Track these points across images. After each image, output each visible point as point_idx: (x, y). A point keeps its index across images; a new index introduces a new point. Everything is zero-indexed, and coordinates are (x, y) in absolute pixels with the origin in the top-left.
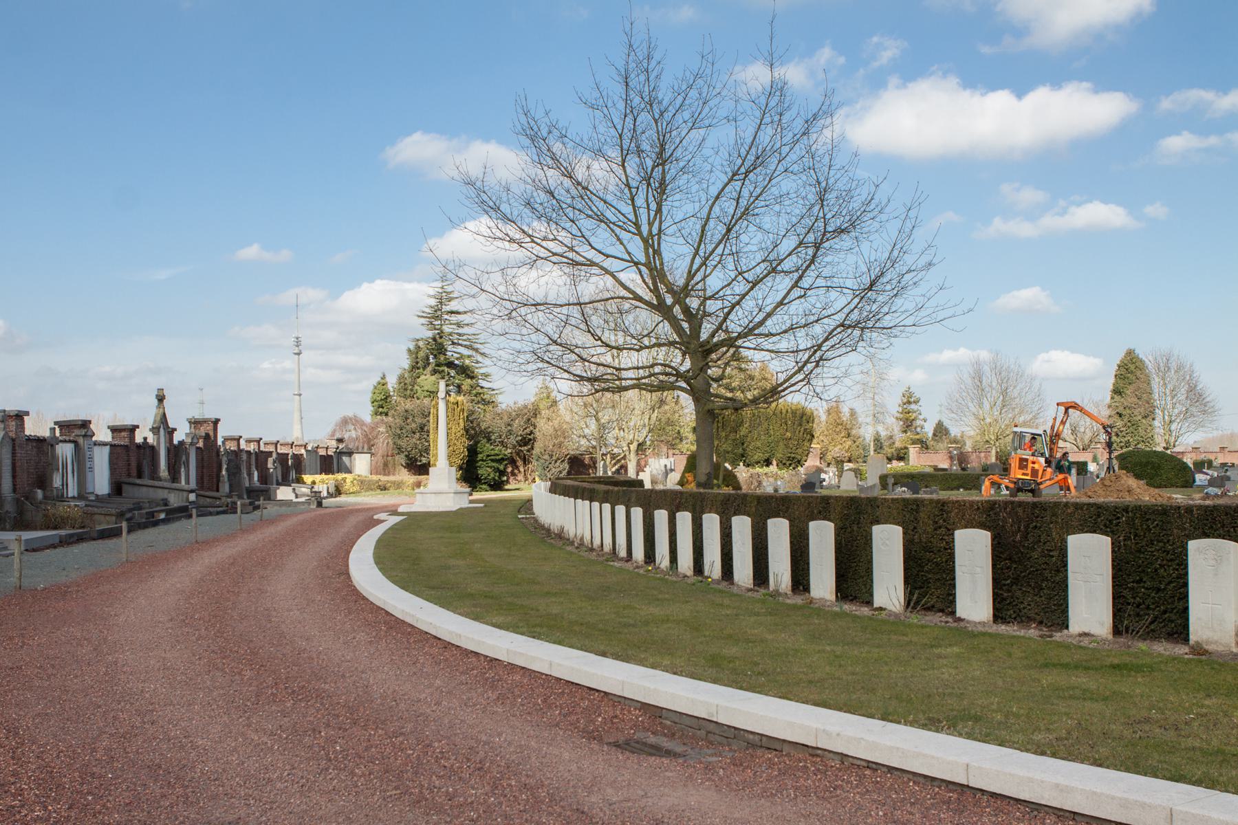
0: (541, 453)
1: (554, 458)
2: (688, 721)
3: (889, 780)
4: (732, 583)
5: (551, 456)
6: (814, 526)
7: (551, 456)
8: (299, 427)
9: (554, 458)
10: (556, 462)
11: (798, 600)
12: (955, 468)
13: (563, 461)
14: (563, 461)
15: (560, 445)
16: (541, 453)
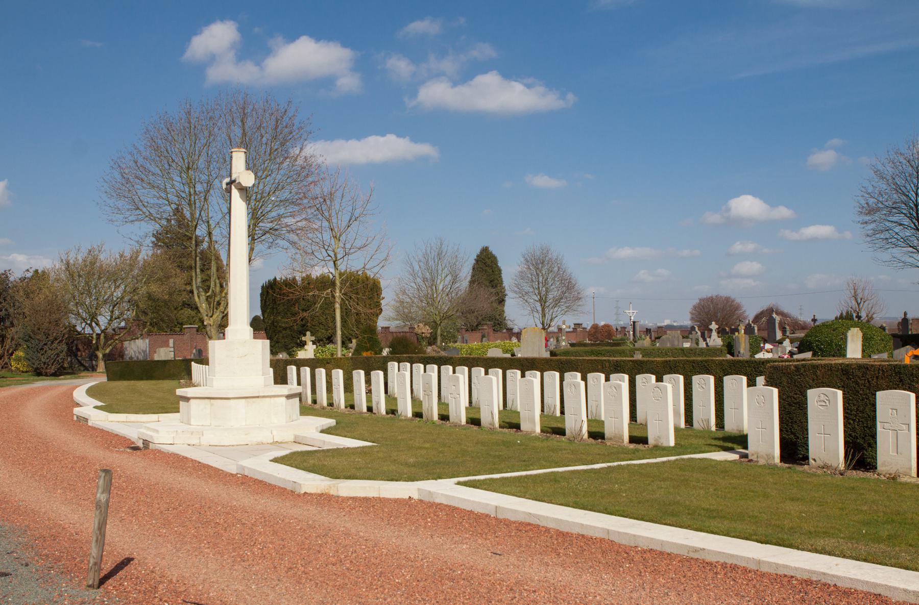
0: (33, 331)
1: (51, 338)
2: (829, 543)
3: (538, 498)
4: (521, 431)
5: (47, 336)
6: (813, 395)
7: (47, 336)
8: (713, 444)
9: (51, 338)
10: (52, 343)
11: (690, 432)
12: (564, 343)
13: (62, 341)
14: (62, 341)
15: (57, 323)
16: (33, 331)
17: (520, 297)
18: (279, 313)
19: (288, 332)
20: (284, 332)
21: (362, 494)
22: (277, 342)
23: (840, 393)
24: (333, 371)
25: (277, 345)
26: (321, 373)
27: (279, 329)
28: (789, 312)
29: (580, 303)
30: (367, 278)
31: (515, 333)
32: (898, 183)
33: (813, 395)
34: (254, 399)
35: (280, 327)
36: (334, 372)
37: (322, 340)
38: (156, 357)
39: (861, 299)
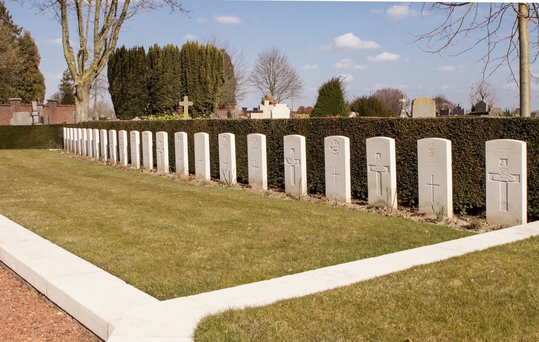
6: (329, 141)
17: (255, 85)
18: (129, 81)
19: (137, 100)
20: (133, 100)
21: (459, 253)
22: (126, 110)
23: (524, 144)
24: (221, 136)
25: (125, 112)
26: (300, 142)
27: (128, 97)
28: (451, 101)
29: (302, 90)
30: (214, 50)
31: (248, 112)
32: (179, 66)
33: (329, 141)
34: (506, 193)
35: (129, 94)
36: (197, 136)
37: (169, 109)
38: (13, 122)
39: (485, 94)
